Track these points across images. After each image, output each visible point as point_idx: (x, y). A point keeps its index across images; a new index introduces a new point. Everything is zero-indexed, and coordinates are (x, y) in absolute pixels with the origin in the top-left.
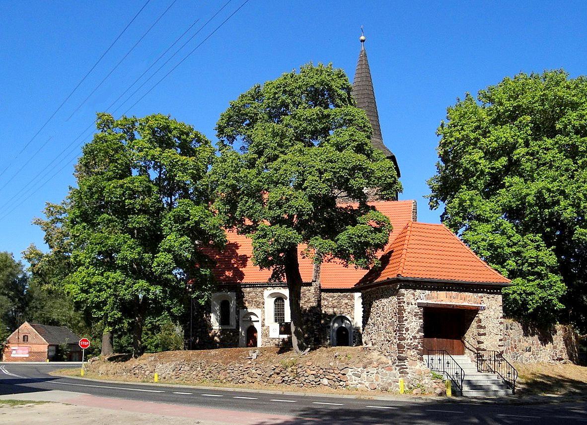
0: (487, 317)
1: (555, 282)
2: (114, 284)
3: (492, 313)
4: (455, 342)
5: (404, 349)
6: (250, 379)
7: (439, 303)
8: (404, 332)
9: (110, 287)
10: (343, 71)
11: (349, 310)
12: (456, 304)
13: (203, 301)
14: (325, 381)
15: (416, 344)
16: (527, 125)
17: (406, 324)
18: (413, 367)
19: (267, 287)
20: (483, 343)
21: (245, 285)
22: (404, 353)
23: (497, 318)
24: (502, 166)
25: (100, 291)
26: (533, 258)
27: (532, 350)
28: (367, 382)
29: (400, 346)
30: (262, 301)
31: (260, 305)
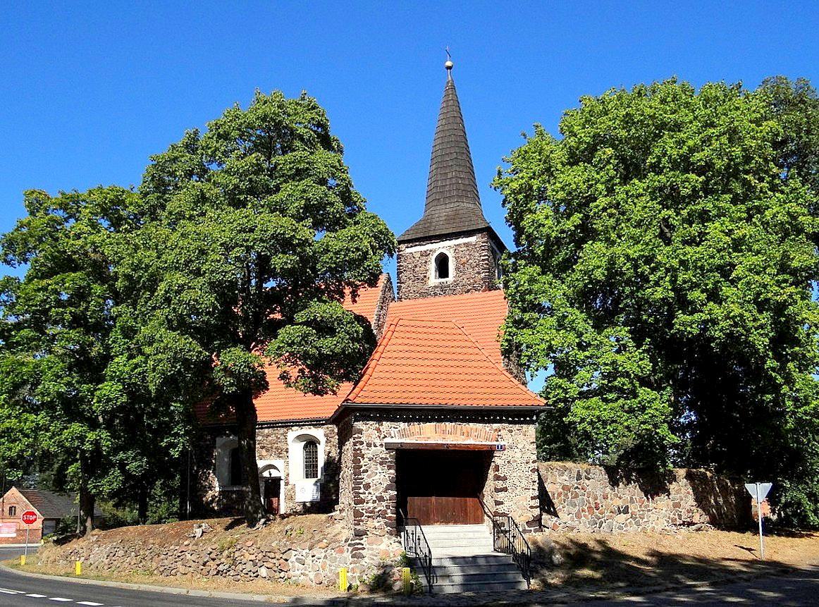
0: (509, 462)
1: (649, 402)
2: (32, 431)
3: (519, 455)
4: (468, 504)
5: (362, 518)
6: (182, 569)
7: (423, 442)
8: (361, 491)
9: (27, 436)
10: (315, 101)
12: (452, 443)
13: (177, 451)
14: (263, 572)
15: (382, 508)
16: (608, 162)
17: (365, 477)
18: (374, 547)
19: (292, 426)
20: (502, 503)
21: (262, 424)
22: (361, 523)
23: (527, 463)
24: (575, 226)
25: (14, 441)
26: (607, 365)
27: (630, 511)
28: (312, 573)
29: (357, 514)
30: (285, 447)
31: (282, 453)
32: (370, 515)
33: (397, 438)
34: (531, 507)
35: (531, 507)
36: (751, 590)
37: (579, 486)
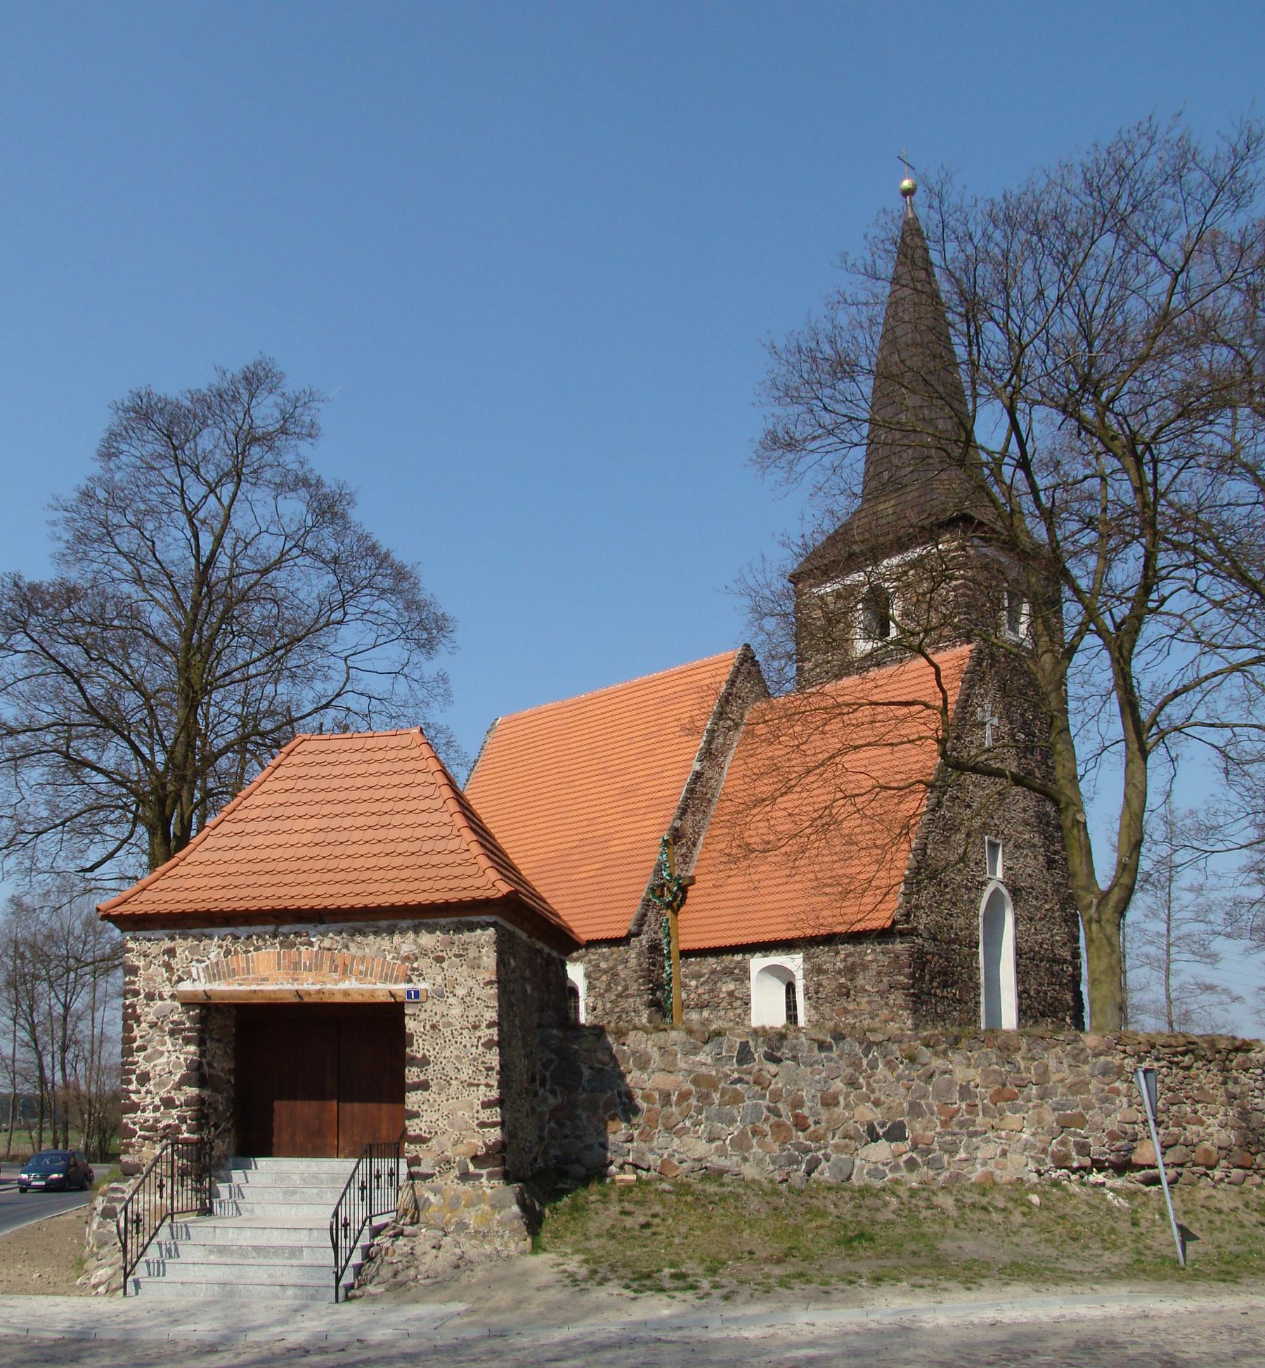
0: (433, 1027)
8: (133, 1087)
11: (738, 1011)
17: (140, 1059)
23: (475, 1027)
32: (147, 1134)
33: (203, 980)
34: (482, 1125)
35: (482, 1125)
36: (460, 1307)
37: (746, 1077)
